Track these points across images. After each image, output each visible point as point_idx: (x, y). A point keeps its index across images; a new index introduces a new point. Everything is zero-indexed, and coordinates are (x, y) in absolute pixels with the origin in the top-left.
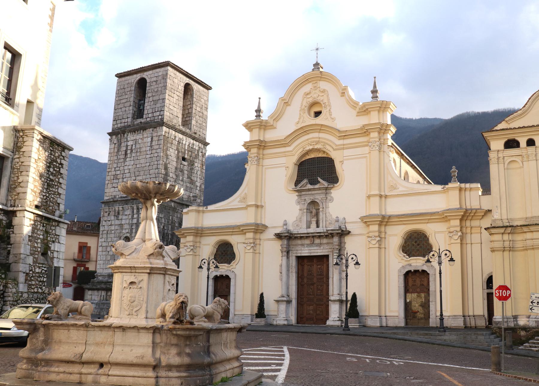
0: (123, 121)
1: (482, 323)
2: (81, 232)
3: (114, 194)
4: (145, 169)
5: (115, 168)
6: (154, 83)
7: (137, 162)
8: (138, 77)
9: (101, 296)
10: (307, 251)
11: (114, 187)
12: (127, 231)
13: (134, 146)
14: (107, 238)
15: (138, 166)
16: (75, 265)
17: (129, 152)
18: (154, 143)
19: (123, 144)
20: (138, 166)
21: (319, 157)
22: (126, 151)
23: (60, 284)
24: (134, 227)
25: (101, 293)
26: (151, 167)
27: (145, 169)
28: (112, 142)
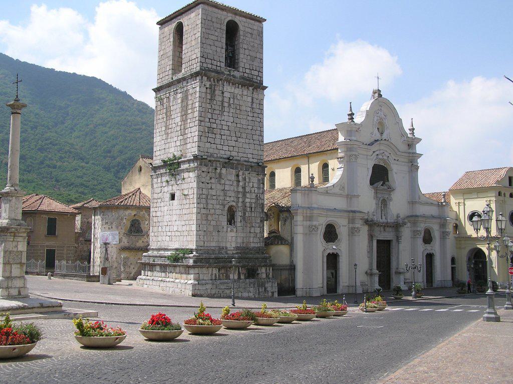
0: (215, 63)
1: (450, 284)
2: (100, 207)
3: (211, 151)
4: (247, 131)
5: (210, 119)
6: (249, 36)
7: (237, 120)
8: (230, 17)
9: (211, 275)
10: (382, 236)
11: (210, 142)
12: (232, 199)
13: (232, 100)
14: (207, 204)
15: (239, 125)
16: (487, 246)
17: (226, 105)
18: (254, 106)
19: (217, 92)
20: (239, 125)
21: (381, 165)
22: (223, 102)
23: (277, 290)
24: (240, 196)
25: (212, 270)
26: (253, 132)
27: (247, 131)
28: (204, 83)
